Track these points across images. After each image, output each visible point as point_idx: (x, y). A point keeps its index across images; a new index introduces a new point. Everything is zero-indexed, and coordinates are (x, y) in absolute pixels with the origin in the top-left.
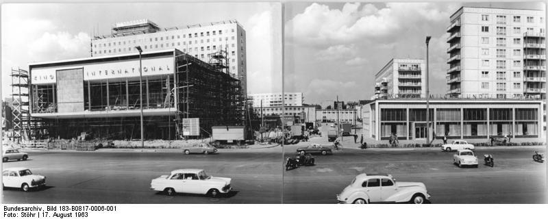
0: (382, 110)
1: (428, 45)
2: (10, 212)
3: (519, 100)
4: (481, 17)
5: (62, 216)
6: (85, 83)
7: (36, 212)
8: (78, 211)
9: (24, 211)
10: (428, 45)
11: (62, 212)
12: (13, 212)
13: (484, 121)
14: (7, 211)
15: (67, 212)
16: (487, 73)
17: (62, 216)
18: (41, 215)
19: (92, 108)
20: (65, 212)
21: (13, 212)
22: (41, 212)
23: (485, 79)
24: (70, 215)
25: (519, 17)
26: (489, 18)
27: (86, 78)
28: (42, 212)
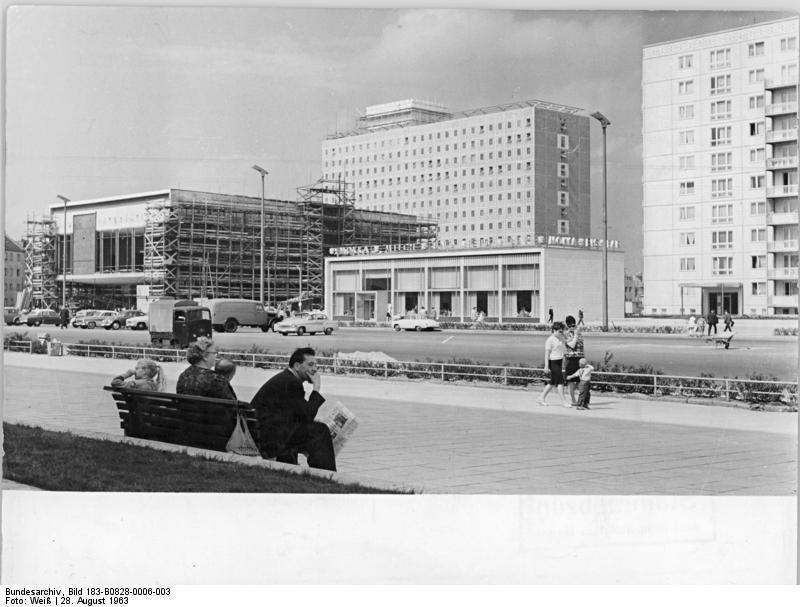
0: (368, 280)
1: (604, 132)
2: (14, 597)
3: (513, 247)
4: (677, 61)
5: (91, 602)
6: (98, 234)
7: (53, 598)
8: (115, 596)
9: (37, 596)
10: (604, 132)
11: (91, 597)
12: (19, 597)
13: (102, 266)
14: (10, 595)
15: (99, 597)
16: (690, 185)
17: (91, 602)
18: (60, 601)
19: (104, 269)
20: (95, 597)
21: (19, 597)
22: (59, 597)
23: (688, 198)
24: (103, 601)
25: (760, 44)
26: (695, 62)
27: (99, 229)
28: (59, 597)
